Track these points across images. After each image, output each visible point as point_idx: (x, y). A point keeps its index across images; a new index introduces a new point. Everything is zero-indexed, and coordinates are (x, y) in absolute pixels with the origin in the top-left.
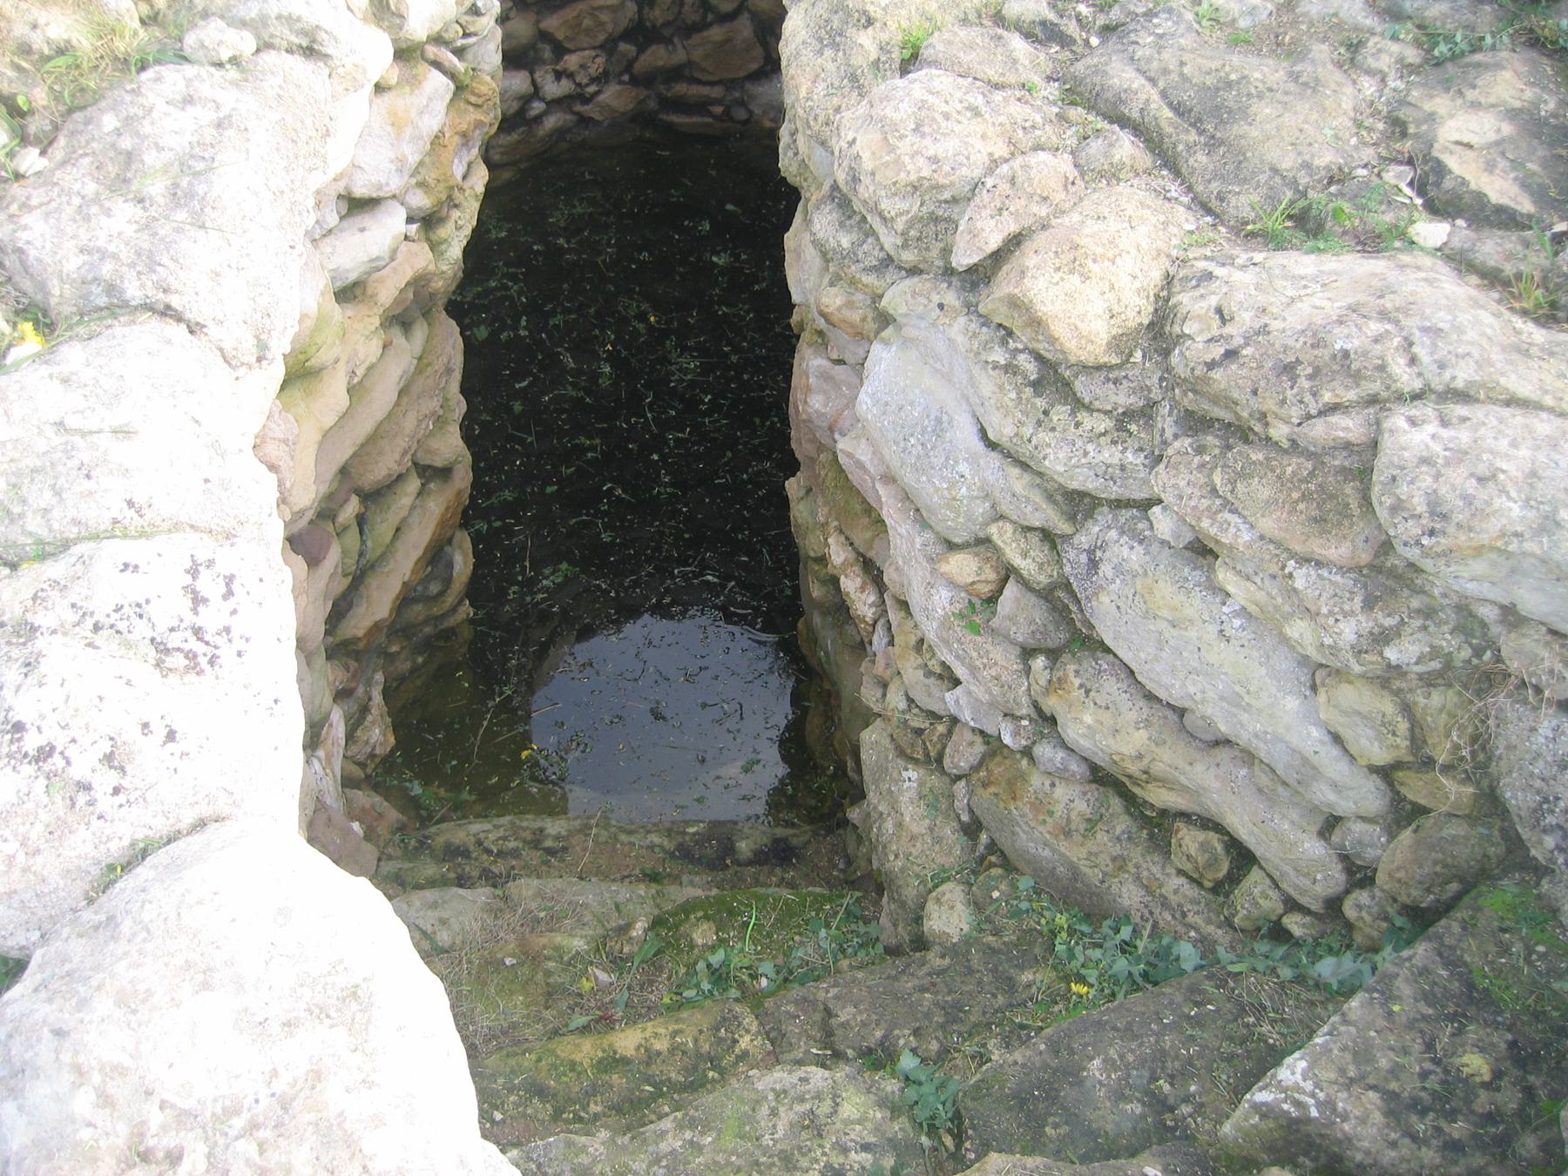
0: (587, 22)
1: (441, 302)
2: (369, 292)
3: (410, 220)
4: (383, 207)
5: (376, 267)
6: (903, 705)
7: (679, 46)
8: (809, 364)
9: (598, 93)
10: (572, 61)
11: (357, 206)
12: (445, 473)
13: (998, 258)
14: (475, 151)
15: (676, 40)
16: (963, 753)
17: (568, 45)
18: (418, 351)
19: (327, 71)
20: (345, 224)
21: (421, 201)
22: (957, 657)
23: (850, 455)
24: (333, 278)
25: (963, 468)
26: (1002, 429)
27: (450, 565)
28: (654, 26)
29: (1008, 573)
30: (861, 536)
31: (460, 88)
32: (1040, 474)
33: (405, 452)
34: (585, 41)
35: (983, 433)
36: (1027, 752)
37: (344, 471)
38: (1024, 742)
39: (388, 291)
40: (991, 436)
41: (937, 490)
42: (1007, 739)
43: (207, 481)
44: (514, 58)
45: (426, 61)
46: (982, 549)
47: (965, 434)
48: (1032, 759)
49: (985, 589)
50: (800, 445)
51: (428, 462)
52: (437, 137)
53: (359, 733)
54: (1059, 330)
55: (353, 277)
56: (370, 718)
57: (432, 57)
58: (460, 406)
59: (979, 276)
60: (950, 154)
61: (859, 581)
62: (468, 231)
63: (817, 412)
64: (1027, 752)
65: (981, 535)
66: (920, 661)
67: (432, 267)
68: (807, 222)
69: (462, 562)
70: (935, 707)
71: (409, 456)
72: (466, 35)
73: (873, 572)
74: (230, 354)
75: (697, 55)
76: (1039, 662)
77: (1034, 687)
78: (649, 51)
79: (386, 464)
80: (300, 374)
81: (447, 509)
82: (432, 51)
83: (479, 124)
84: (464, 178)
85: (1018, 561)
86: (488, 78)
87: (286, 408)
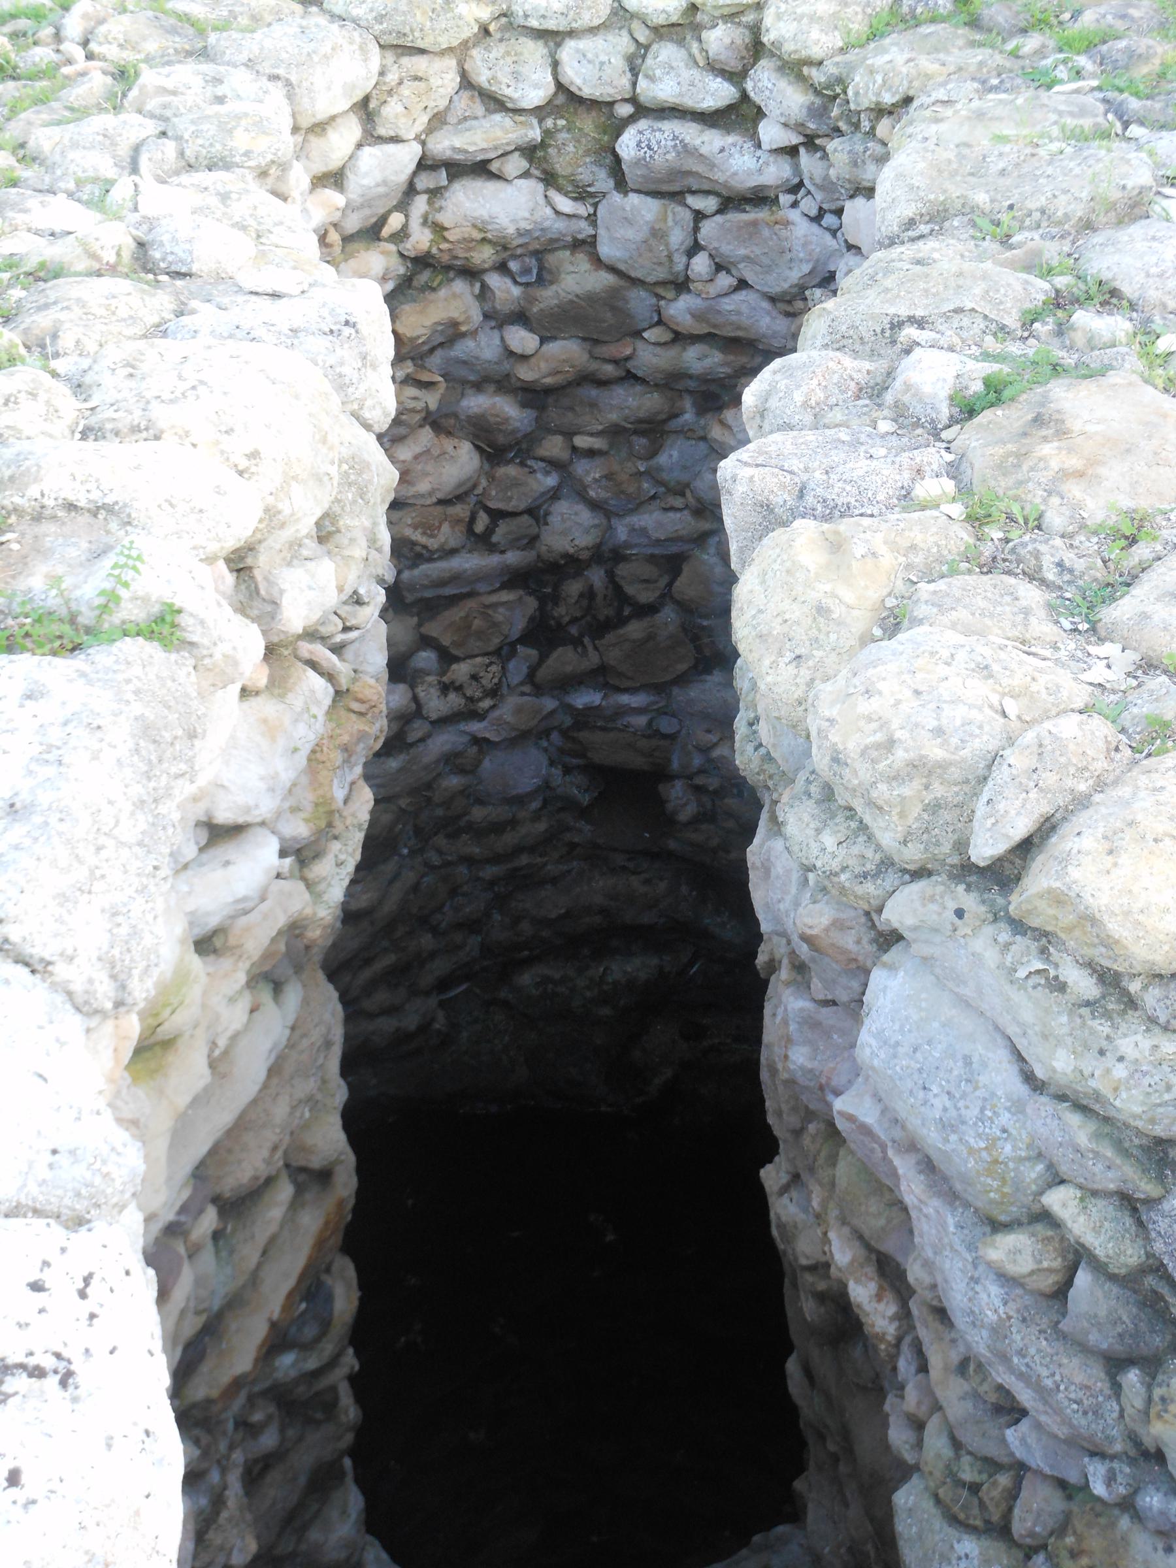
0: (477, 623)
1: (317, 956)
2: (232, 941)
3: (283, 854)
4: (251, 831)
5: (242, 909)
6: (948, 1452)
7: (590, 648)
8: (786, 1007)
9: (493, 707)
10: (461, 671)
11: (219, 834)
12: (324, 1176)
13: (1026, 847)
14: (358, 770)
15: (586, 640)
16: (1034, 1510)
17: (455, 652)
18: (291, 1019)
19: (192, 662)
20: (204, 857)
21: (299, 829)
22: (1021, 1376)
23: (851, 1118)
24: (191, 924)
25: (1005, 1118)
26: (1060, 1063)
27: (329, 1299)
28: (559, 624)
29: (1076, 1256)
30: (873, 1217)
31: (339, 694)
32: (1107, 1120)
33: (275, 1148)
34: (474, 645)
35: (1029, 1077)
36: (1127, 1505)
37: (200, 1173)
38: (1122, 1490)
39: (258, 938)
40: (1040, 1073)
41: (971, 1151)
42: (1099, 1489)
43: (54, 1152)
44: (398, 669)
45: (300, 660)
46: (1039, 1228)
47: (1002, 1078)
48: (1137, 1516)
49: (1047, 1283)
50: (779, 1117)
51: (302, 1163)
52: (313, 752)
53: (211, 1535)
54: (1115, 927)
55: (213, 922)
56: (224, 1515)
57: (306, 655)
58: (340, 1094)
59: (1004, 873)
60: (958, 723)
61: (873, 1287)
62: (350, 867)
63: (802, 1068)
64: (1127, 1505)
65: (1036, 1208)
66: (966, 1387)
67: (308, 911)
68: (777, 825)
69: (344, 1299)
70: (992, 1450)
71: (279, 1154)
72: (346, 629)
73: (890, 1273)
74: (79, 1000)
75: (614, 656)
76: (1132, 1377)
77: (1129, 1411)
78: (555, 655)
79: (252, 1164)
80: (151, 1051)
81: (327, 1223)
82: (307, 649)
83: (362, 736)
84: (346, 802)
85: (1091, 1240)
86: (372, 682)
87: (135, 1079)
